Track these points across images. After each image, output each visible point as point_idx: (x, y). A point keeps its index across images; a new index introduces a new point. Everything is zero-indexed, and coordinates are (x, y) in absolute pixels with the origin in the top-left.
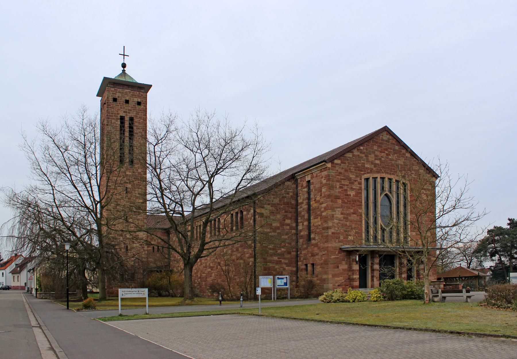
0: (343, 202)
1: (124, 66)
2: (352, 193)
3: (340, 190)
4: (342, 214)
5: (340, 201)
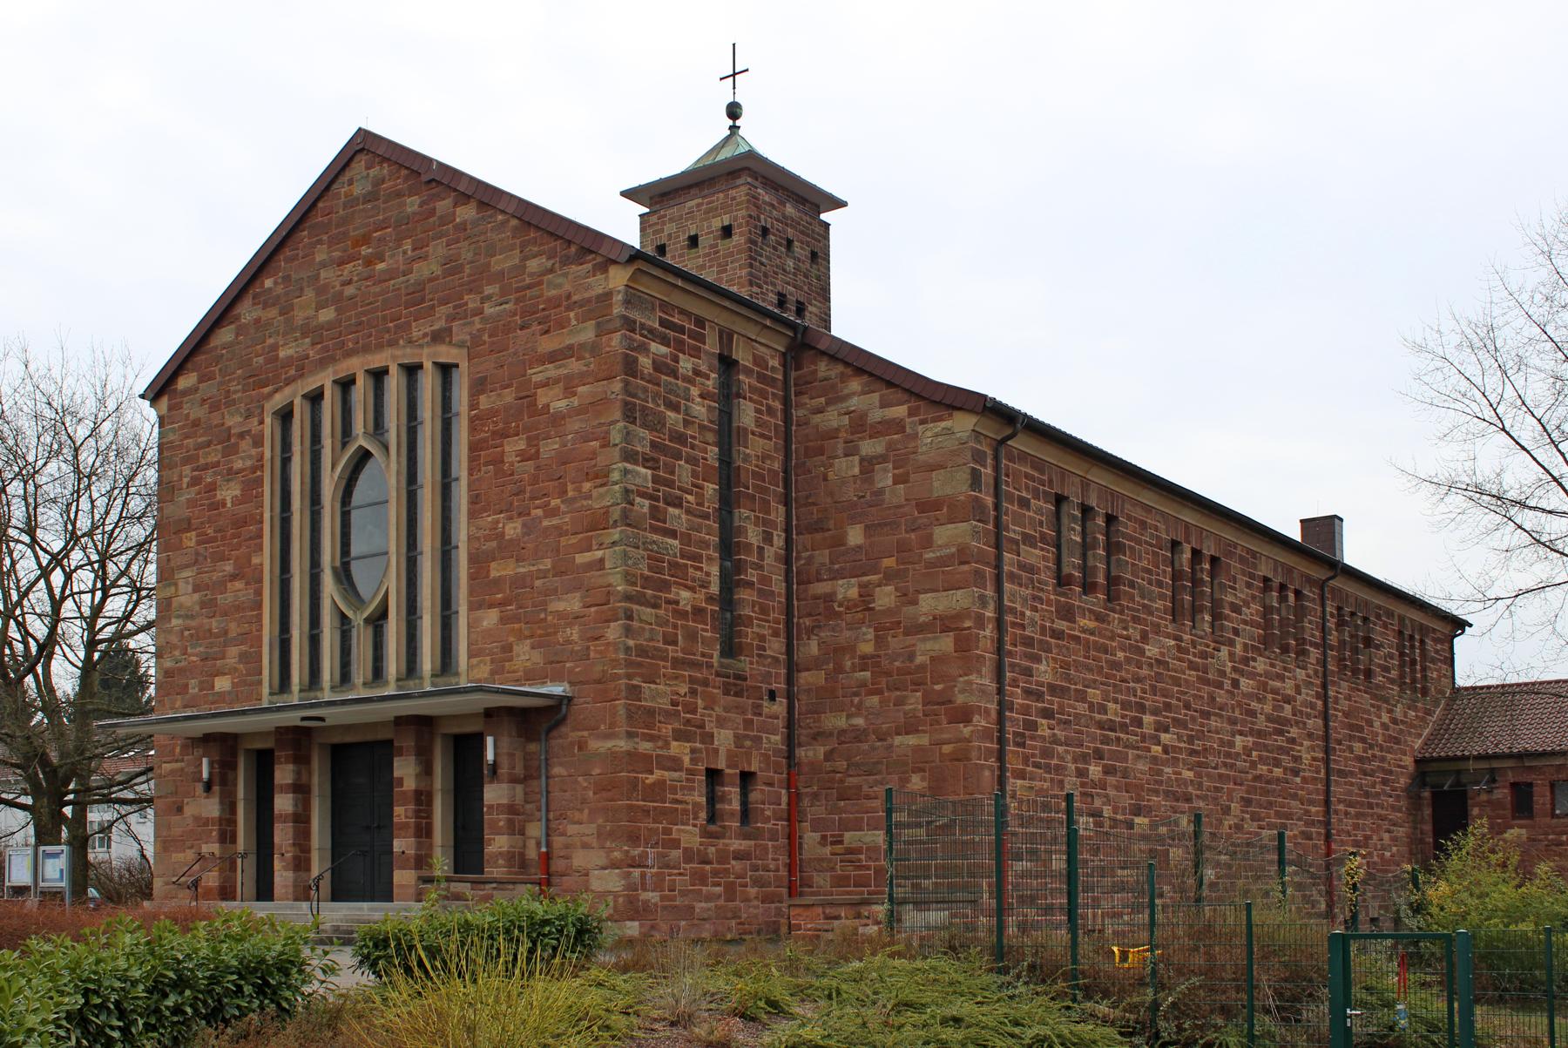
0: (204, 540)
1: (734, 111)
2: (229, 493)
3: (192, 493)
4: (196, 589)
5: (190, 540)
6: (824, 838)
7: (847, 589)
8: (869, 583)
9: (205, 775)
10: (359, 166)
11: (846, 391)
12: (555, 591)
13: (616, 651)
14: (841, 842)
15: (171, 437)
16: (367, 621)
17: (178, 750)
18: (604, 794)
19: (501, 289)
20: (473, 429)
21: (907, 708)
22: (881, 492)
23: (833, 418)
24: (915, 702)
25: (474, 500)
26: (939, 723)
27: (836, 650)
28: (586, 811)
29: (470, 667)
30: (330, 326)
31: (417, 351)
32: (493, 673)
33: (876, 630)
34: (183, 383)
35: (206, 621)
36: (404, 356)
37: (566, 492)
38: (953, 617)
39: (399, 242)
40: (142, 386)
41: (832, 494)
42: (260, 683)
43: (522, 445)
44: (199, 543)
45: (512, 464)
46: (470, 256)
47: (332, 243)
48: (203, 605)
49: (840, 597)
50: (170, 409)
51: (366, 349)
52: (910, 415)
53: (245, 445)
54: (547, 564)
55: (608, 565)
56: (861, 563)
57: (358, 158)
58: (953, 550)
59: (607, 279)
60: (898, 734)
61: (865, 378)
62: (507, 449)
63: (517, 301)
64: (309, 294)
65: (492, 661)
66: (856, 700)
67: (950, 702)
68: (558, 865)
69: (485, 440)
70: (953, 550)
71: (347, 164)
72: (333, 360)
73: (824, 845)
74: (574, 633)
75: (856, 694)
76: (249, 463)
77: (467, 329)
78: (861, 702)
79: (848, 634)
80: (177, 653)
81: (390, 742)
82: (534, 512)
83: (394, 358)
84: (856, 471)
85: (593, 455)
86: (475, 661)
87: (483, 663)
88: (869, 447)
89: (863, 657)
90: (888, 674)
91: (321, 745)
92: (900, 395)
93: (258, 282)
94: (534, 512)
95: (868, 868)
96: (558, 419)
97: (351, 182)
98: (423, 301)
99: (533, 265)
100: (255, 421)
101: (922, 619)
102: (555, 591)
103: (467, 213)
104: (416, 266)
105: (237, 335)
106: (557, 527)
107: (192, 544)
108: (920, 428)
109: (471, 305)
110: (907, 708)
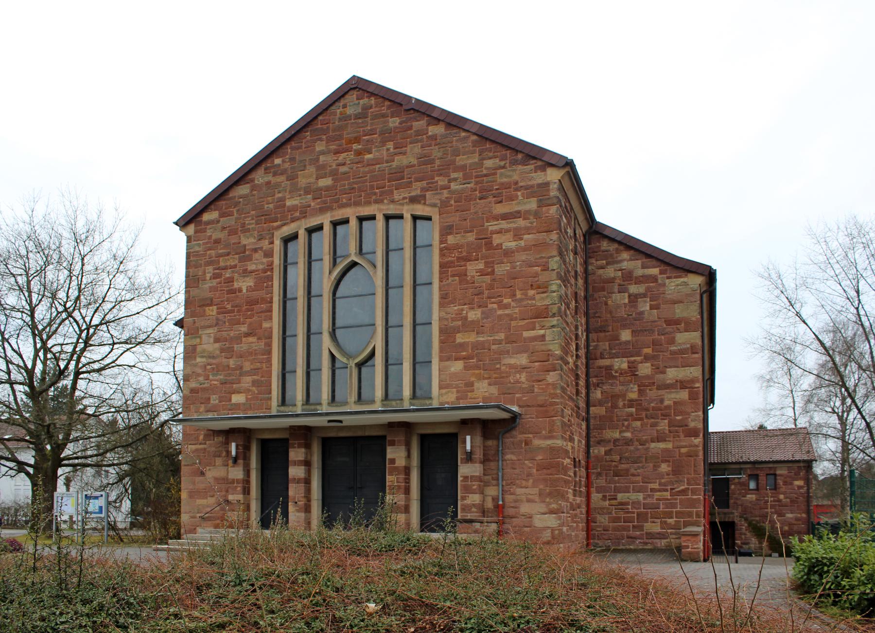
0: (222, 311)
4: (217, 340)
5: (212, 311)
6: (604, 496)
7: (621, 364)
8: (635, 361)
9: (234, 453)
10: (352, 97)
11: (619, 258)
12: (508, 352)
13: (555, 388)
14: (616, 499)
15: (197, 249)
16: (356, 364)
17: (201, 437)
18: (545, 471)
19: (464, 175)
20: (442, 255)
21: (659, 428)
22: (642, 313)
23: (610, 272)
24: (664, 425)
25: (443, 297)
26: (679, 437)
27: (612, 396)
28: (531, 481)
29: (440, 395)
30: (327, 189)
31: (398, 207)
32: (458, 398)
33: (639, 386)
34: (206, 217)
35: (224, 360)
36: (388, 209)
37: (515, 295)
38: (688, 381)
39: (383, 143)
40: (176, 218)
41: (611, 312)
42: (270, 399)
43: (481, 266)
44: (218, 313)
45: (473, 277)
46: (440, 154)
47: (329, 140)
48: (222, 350)
49: (616, 367)
50: (196, 232)
51: (357, 204)
52: (661, 273)
53: (258, 256)
54: (502, 336)
55: (547, 338)
56: (627, 351)
57: (351, 93)
58: (688, 346)
59: (545, 175)
60: (653, 441)
61: (632, 252)
62: (469, 268)
63: (477, 183)
64: (311, 169)
65: (458, 392)
66: (626, 423)
67: (686, 426)
68: (510, 511)
69: (452, 262)
70: (688, 346)
71: (343, 96)
72: (330, 209)
73: (605, 500)
74: (523, 377)
75: (626, 420)
76: (261, 267)
77: (438, 197)
78: (629, 425)
79: (621, 388)
80: (201, 379)
81: (384, 438)
82: (490, 306)
83: (380, 210)
84: (626, 301)
85: (536, 275)
86: (444, 391)
87: (445, 391)
88: (634, 289)
89: (631, 401)
90: (647, 410)
91: (258, 439)
92: (654, 262)
93: (270, 161)
94: (490, 306)
95: (633, 513)
96: (508, 253)
97: (345, 106)
98: (403, 178)
99: (489, 163)
100: (267, 242)
101: (668, 382)
102: (508, 352)
103: (438, 130)
104: (396, 158)
105: (252, 190)
106: (508, 315)
107: (214, 313)
108: (667, 281)
109: (440, 183)
110: (659, 428)
